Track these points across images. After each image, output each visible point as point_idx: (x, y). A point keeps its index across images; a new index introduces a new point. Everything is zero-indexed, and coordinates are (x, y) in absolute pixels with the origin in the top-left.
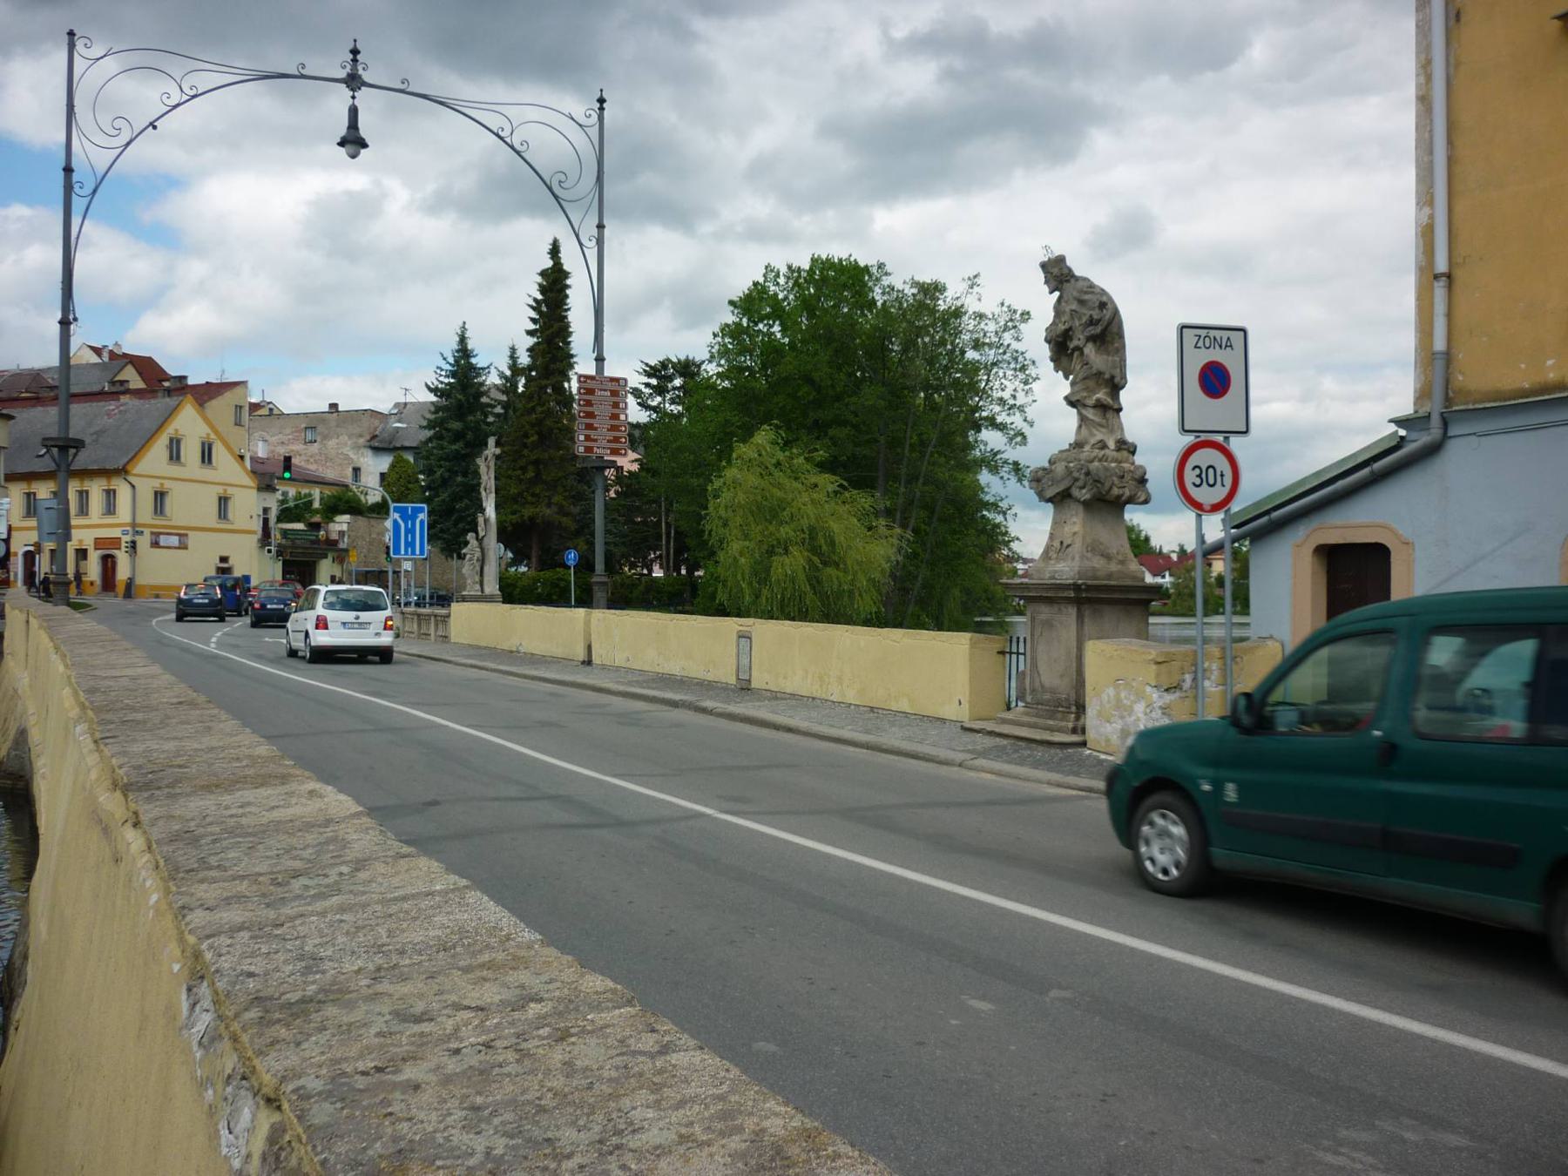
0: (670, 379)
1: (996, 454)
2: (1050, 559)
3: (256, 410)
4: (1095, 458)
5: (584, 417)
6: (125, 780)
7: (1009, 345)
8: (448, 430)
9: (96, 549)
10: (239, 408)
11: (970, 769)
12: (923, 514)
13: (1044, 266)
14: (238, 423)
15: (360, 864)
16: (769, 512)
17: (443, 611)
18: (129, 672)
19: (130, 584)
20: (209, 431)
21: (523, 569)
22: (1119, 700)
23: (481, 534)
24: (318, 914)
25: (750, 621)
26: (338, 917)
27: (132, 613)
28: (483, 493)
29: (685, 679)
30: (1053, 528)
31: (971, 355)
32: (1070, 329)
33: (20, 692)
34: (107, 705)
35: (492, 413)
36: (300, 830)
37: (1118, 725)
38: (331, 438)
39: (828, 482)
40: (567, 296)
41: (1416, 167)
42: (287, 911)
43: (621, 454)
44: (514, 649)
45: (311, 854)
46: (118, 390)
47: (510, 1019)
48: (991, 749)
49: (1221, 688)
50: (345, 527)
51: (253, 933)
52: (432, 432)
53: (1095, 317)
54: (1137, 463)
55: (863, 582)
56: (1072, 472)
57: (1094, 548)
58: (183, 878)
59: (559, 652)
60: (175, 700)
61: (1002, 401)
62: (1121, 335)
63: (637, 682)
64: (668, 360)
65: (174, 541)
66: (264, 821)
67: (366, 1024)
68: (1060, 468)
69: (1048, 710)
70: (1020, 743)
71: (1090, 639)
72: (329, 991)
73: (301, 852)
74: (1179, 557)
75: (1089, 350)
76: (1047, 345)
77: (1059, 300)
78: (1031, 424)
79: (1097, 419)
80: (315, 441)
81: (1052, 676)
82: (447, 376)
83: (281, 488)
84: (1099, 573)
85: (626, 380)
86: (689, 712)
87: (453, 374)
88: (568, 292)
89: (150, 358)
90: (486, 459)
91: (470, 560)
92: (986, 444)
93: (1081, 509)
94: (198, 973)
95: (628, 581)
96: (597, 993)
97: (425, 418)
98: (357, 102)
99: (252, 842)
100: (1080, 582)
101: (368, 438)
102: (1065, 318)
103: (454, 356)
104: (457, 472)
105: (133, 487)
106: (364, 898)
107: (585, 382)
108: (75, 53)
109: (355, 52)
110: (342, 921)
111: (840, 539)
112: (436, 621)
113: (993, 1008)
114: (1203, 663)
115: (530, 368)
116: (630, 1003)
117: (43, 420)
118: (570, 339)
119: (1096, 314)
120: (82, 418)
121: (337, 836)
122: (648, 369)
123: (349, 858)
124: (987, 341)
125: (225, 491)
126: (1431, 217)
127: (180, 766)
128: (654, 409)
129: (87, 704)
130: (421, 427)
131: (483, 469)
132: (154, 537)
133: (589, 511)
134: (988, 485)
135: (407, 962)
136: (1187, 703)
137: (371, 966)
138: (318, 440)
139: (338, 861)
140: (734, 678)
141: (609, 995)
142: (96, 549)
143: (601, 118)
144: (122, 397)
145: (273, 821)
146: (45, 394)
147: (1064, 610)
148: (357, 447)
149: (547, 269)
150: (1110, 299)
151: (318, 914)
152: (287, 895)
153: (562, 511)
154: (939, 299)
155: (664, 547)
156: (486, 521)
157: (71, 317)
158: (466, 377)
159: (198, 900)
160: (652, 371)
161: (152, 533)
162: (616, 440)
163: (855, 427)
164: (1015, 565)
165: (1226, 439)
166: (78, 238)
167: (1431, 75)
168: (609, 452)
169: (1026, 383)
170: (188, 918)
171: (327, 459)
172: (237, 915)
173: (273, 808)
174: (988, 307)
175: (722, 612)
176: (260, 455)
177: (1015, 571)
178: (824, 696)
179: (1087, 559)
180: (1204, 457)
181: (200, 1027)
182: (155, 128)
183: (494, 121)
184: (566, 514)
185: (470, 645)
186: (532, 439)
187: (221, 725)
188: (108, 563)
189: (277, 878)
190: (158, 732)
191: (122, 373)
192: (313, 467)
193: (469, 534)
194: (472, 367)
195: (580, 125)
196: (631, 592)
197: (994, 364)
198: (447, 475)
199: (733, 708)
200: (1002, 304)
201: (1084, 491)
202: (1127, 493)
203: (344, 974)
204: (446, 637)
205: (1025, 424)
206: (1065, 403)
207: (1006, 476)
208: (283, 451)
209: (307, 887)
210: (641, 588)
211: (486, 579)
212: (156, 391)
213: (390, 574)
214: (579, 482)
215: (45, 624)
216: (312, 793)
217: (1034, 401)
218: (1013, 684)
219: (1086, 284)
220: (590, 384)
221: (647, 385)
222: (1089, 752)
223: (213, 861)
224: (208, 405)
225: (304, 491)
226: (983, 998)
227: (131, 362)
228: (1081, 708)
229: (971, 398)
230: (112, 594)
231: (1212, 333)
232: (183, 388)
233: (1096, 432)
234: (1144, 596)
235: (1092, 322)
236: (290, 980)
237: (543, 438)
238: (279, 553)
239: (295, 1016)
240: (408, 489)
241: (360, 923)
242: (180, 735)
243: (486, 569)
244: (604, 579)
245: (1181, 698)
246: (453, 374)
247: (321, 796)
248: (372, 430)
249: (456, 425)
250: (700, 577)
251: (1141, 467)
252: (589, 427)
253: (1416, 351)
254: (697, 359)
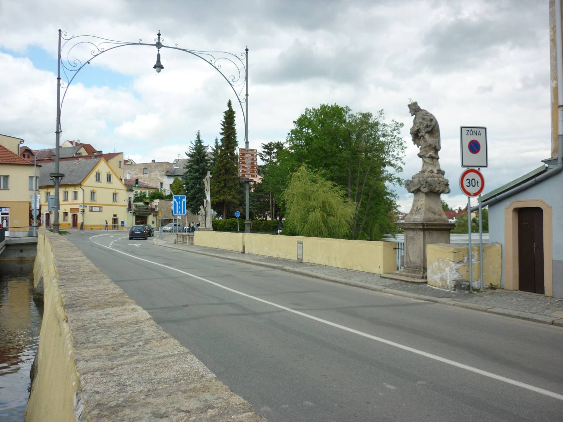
0: (272, 149)
1: (391, 175)
2: (413, 214)
3: (126, 163)
4: (429, 176)
5: (241, 164)
6: (65, 304)
7: (396, 136)
8: (193, 169)
9: (70, 212)
10: (120, 162)
11: (385, 292)
12: (365, 197)
13: (409, 106)
14: (120, 167)
15: (147, 342)
16: (306, 196)
17: (192, 234)
18: (74, 259)
19: (82, 225)
20: (110, 170)
21: (220, 218)
22: (439, 267)
23: (205, 206)
24: (128, 364)
25: (302, 237)
26: (136, 365)
27: (82, 235)
28: (206, 192)
29: (279, 258)
30: (414, 202)
31: (382, 139)
32: (419, 129)
33: (42, 264)
34: (64, 272)
35: (209, 163)
36: (126, 326)
37: (439, 276)
38: (153, 172)
39: (329, 184)
40: (234, 120)
41: (551, 66)
42: (116, 362)
43: (255, 177)
44: (217, 248)
45: (129, 336)
46: (79, 156)
47: (200, 417)
48: (391, 285)
49: (478, 262)
50: (157, 204)
51: (102, 373)
52: (188, 169)
53: (429, 124)
54: (445, 178)
55: (343, 222)
56: (421, 182)
57: (429, 210)
58: (79, 347)
59: (233, 249)
60: (89, 270)
61: (393, 156)
62: (438, 131)
63: (261, 259)
64: (271, 142)
65: (98, 209)
66: (113, 321)
67: (140, 418)
68: (416, 180)
69: (412, 270)
70: (402, 282)
71: (428, 244)
72: (128, 401)
73: (125, 335)
74: (458, 212)
75: (427, 136)
76: (411, 135)
77: (415, 118)
78: (404, 164)
79: (430, 162)
80: (147, 173)
81: (414, 258)
82: (193, 150)
83: (135, 190)
84: (432, 219)
85: (256, 150)
86: (279, 271)
87: (195, 149)
88: (235, 119)
89: (90, 145)
90: (207, 179)
91: (201, 215)
92: (388, 172)
93: (424, 196)
94: (80, 390)
95: (258, 222)
96: (236, 405)
97: (185, 165)
98: (160, 52)
99: (107, 331)
100: (424, 222)
101: (166, 172)
102: (418, 125)
103: (196, 143)
104: (197, 184)
105: (83, 190)
106: (147, 357)
107: (242, 151)
108: (61, 38)
110: (137, 367)
111: (335, 206)
112: (189, 238)
113: (396, 388)
114: (471, 252)
115: (222, 146)
116: (250, 410)
117: (50, 167)
118: (236, 136)
119: (429, 124)
120: (64, 167)
121: (140, 329)
122: (264, 146)
123: (143, 339)
124: (388, 134)
125: (115, 191)
126: (557, 84)
127: (86, 298)
128: (267, 160)
129: (57, 271)
130: (184, 168)
131: (206, 183)
132: (90, 208)
133: (244, 197)
134: (388, 186)
135: (161, 387)
136: (466, 267)
137: (146, 390)
138: (148, 173)
139: (139, 340)
140: (297, 258)
141: (241, 406)
142: (70, 212)
143: (247, 56)
144: (79, 159)
145: (116, 322)
146: (53, 158)
147: (418, 233)
148: (161, 175)
149: (227, 111)
150: (434, 118)
151: (128, 364)
152: (117, 355)
153: (234, 198)
154: (369, 119)
155: (271, 210)
156: (207, 201)
157: (60, 130)
158: (200, 150)
159: (83, 357)
160: (266, 147)
161: (90, 206)
162: (253, 172)
163: (340, 166)
164: (398, 215)
165: (479, 169)
166: (62, 103)
167: (555, 31)
168: (250, 176)
169: (402, 149)
170: (77, 365)
171: (152, 179)
172: (97, 364)
173: (117, 316)
174: (388, 121)
175: (293, 234)
176: (128, 178)
177: (398, 217)
178: (329, 265)
179: (427, 214)
180: (471, 176)
181: (80, 411)
182: (89, 63)
184: (236, 198)
185: (201, 246)
186: (223, 171)
187: (104, 281)
188: (75, 217)
189: (114, 347)
190: (80, 283)
191: (80, 150)
192: (146, 182)
193: (201, 206)
194: (202, 146)
195: (239, 59)
196: (259, 227)
197: (391, 142)
198: (193, 185)
199: (295, 269)
200: (393, 121)
201: (425, 189)
202: (441, 189)
203: (135, 393)
204: (193, 243)
205: (402, 164)
206: (417, 156)
207: (395, 183)
208: (136, 177)
209: (126, 351)
210: (263, 225)
211: (207, 222)
212: (91, 156)
213: (173, 220)
214: (241, 187)
215: (49, 240)
216: (133, 309)
217: (405, 156)
218: (400, 259)
219: (425, 112)
220: (244, 152)
221: (264, 152)
222: (428, 286)
223: (91, 339)
224: (109, 161)
225: (143, 191)
226: (392, 384)
227: (83, 146)
228: (425, 269)
229: (382, 155)
230: (76, 228)
231: (473, 129)
232: (101, 155)
233: (429, 166)
234: (449, 228)
235: (427, 126)
236: (113, 396)
237: (227, 171)
238: (134, 213)
239: (112, 413)
240: (180, 190)
241: (144, 369)
242: (88, 284)
243: (207, 218)
244: (249, 222)
245: (463, 265)
246: (195, 149)
247: (136, 311)
248: (167, 169)
249: (196, 167)
250: (283, 221)
251: (447, 179)
252: (243, 167)
253: (552, 134)
254: (282, 142)
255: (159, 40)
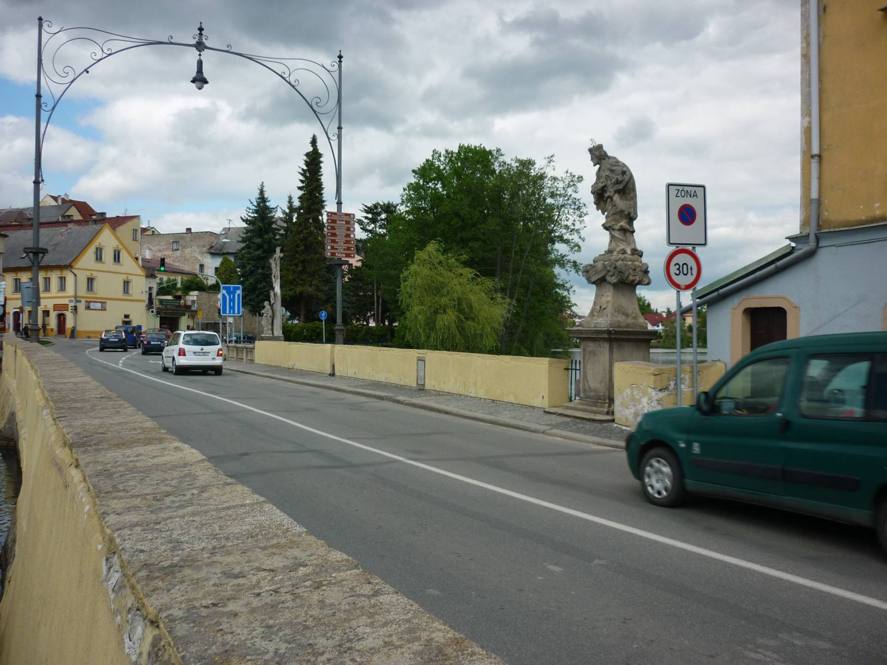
0: (379, 214)
1: (563, 257)
2: (594, 316)
3: (145, 232)
4: (619, 259)
5: (330, 236)
6: (71, 441)
7: (571, 195)
8: (253, 243)
9: (54, 310)
10: (135, 231)
11: (549, 435)
12: (522, 291)
13: (590, 150)
14: (135, 239)
15: (204, 489)
16: (435, 289)
17: (251, 346)
18: (73, 380)
19: (73, 330)
20: (118, 244)
21: (296, 322)
22: (633, 396)
23: (272, 302)
24: (180, 517)
25: (424, 351)
26: (191, 518)
27: (74, 347)
28: (273, 279)
29: (387, 384)
30: (596, 299)
31: (549, 201)
32: (605, 186)
33: (11, 391)
34: (60, 399)
35: (278, 234)
36: (170, 470)
37: (632, 410)
38: (187, 248)
39: (468, 272)
40: (321, 168)
41: (801, 94)
42: (162, 515)
43: (351, 257)
44: (291, 367)
45: (176, 483)
46: (67, 221)
47: (288, 576)
48: (560, 424)
49: (690, 389)
50: (195, 298)
51: (143, 528)
52: (244, 244)
53: (620, 179)
54: (643, 262)
55: (488, 329)
56: (606, 267)
57: (619, 310)
58: (103, 497)
59: (316, 369)
60: (99, 396)
61: (567, 227)
62: (634, 190)
63: (360, 385)
64: (378, 203)
65: (99, 306)
66: (150, 464)
67: (207, 579)
68: (599, 265)
69: (593, 402)
70: (577, 420)
71: (616, 361)
72: (186, 560)
73: (170, 482)
74: (667, 315)
75: (616, 198)
76: (592, 195)
77: (599, 170)
78: (583, 240)
79: (621, 237)
80: (178, 250)
81: (595, 382)
82: (253, 213)
83: (159, 276)
84: (622, 324)
85: (354, 215)
86: (390, 403)
87: (256, 212)
88: (321, 165)
89: (85, 202)
90: (275, 260)
91: (266, 316)
92: (558, 251)
93: (611, 288)
94: (112, 550)
95: (355, 329)
96: (337, 561)
97: (240, 236)
98: (202, 58)
99: (142, 476)
100: (611, 329)
101: (208, 247)
102: (603, 180)
103: (257, 202)
104: (258, 267)
105: (75, 275)
106: (206, 508)
107: (331, 216)
108: (43, 30)
109: (201, 29)
110: (193, 521)
111: (475, 305)
112: (247, 351)
113: (562, 570)
114: (681, 375)
115: (300, 208)
116: (356, 567)
117: (25, 237)
118: (322, 192)
119: (620, 178)
120: (46, 236)
121: (191, 473)
122: (366, 208)
123: (197, 485)
124: (559, 193)
125: (127, 277)
126: (810, 123)
127: (102, 433)
128: (370, 231)
129: (49, 398)
130: (238, 242)
131: (273, 265)
132: (87, 304)
133: (333, 289)
134: (559, 274)
135: (230, 544)
136: (671, 397)
137: (210, 547)
138: (180, 249)
139: (191, 487)
140: (415, 383)
141: (344, 563)
142: (54, 310)
143: (340, 67)
144: (69, 224)
145: (154, 464)
146: (25, 223)
147: (602, 345)
148: (202, 253)
149: (310, 152)
150: (628, 169)
151: (180, 517)
152: (162, 506)
153: (318, 289)
154: (531, 169)
155: (376, 310)
156: (275, 295)
157: (40, 179)
158: (264, 213)
159: (112, 509)
160: (369, 210)
161: (86, 301)
162: (349, 249)
163: (484, 241)
164: (574, 319)
165: (694, 248)
166: (44, 134)
167: (809, 42)
168: (344, 255)
169: (580, 216)
170: (107, 519)
171: (185, 260)
172: (134, 517)
173: (154, 457)
174: (559, 174)
175: (409, 346)
176: (147, 257)
177: (574, 323)
178: (466, 394)
179: (615, 316)
180: (681, 258)
181: (113, 581)
182: (88, 72)
183: (279, 69)
184: (320, 291)
185: (266, 365)
186: (301, 248)
187: (125, 410)
188: (61, 319)
189: (156, 497)
190: (89, 414)
191: (69, 211)
192: (177, 264)
193: (266, 302)
194: (267, 208)
195: (328, 71)
196: (357, 335)
197: (562, 206)
198: (253, 269)
199: (414, 401)
200: (567, 172)
201: (613, 278)
202: (638, 279)
203: (194, 551)
204: (252, 360)
205: (580, 240)
206: (602, 228)
207: (569, 269)
208: (160, 255)
209: (173, 502)
210: (363, 332)
211: (275, 327)
212: (88, 221)
213: (221, 324)
214: (328, 272)
215: (25, 353)
216: (176, 448)
217: (585, 227)
218: (573, 387)
219: (614, 161)
220: (334, 217)
221: (366, 218)
222: (616, 425)
223: (121, 487)
224: (117, 229)
225: (172, 278)
226: (556, 564)
227: (74, 205)
228: (611, 400)
229: (549, 225)
230: (64, 336)
231: (686, 188)
232: (104, 220)
233: (620, 244)
234: (647, 337)
235: (618, 182)
236: (164, 554)
237: (307, 248)
238: (158, 313)
239: (167, 574)
240: (231, 277)
241: (204, 522)
242: (102, 416)
243: (275, 322)
244: (342, 328)
245: (668, 394)
246: (256, 212)
247: (182, 450)
248: (210, 243)
249: (258, 240)
250: (396, 326)
251: (646, 264)
252: (333, 241)
253: (801, 198)
254: (395, 203)
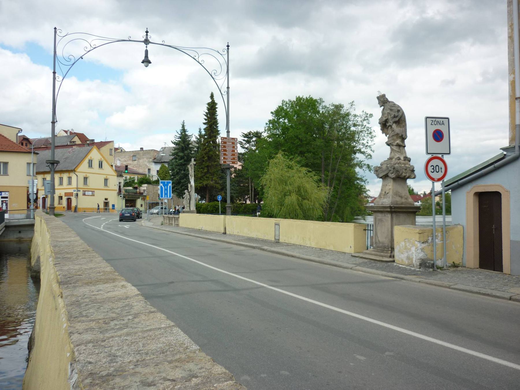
0: (252, 138)
1: (361, 162)
2: (381, 198)
3: (116, 151)
4: (397, 163)
5: (223, 151)
6: (60, 281)
7: (365, 125)
8: (178, 156)
9: (65, 196)
10: (111, 150)
11: (355, 270)
12: (337, 182)
13: (378, 98)
14: (111, 155)
15: (136, 316)
16: (283, 181)
17: (177, 216)
18: (69, 239)
19: (76, 208)
20: (101, 157)
21: (204, 202)
22: (406, 246)
23: (189, 190)
24: (119, 336)
25: (279, 219)
26: (125, 338)
27: (76, 217)
28: (190, 177)
29: (257, 239)
30: (382, 187)
31: (353, 129)
32: (387, 119)
33: (38, 244)
34: (59, 252)
35: (193, 150)
36: (117, 301)
37: (406, 255)
38: (141, 159)
39: (304, 170)
40: (217, 111)
41: (509, 61)
42: (107, 335)
43: (235, 164)
44: (200, 229)
45: (119, 311)
46: (73, 144)
47: (184, 386)
48: (361, 263)
49: (442, 242)
50: (145, 188)
51: (94, 344)
52: (174, 157)
53: (396, 115)
54: (411, 165)
55: (317, 205)
56: (388, 168)
57: (397, 194)
58: (73, 320)
59: (215, 230)
60: (82, 250)
61: (363, 144)
62: (405, 121)
63: (241, 240)
64: (251, 132)
65: (90, 193)
66: (105, 297)
67: (130, 386)
68: (384, 167)
69: (381, 250)
70: (372, 261)
71: (395, 225)
72: (118, 371)
73: (115, 310)
74: (423, 196)
75: (394, 126)
76: (379, 125)
77: (383, 109)
78: (373, 151)
79: (397, 150)
80: (136, 160)
81: (383, 238)
82: (178, 138)
83: (125, 176)
84: (399, 203)
85: (237, 139)
86: (258, 250)
87: (180, 138)
88: (217, 110)
89: (83, 134)
90: (191, 166)
91: (186, 199)
92: (358, 159)
93: (392, 181)
94: (74, 361)
95: (238, 206)
96: (218, 374)
97: (171, 153)
98: (148, 48)
99: (99, 306)
100: (392, 206)
101: (153, 159)
102: (386, 115)
103: (181, 132)
104: (182, 170)
105: (77, 176)
106: (136, 330)
107: (223, 139)
108: (57, 35)
110: (127, 340)
111: (309, 191)
112: (175, 220)
113: (365, 359)
114: (435, 233)
115: (205, 135)
116: (231, 379)
117: (46, 154)
118: (218, 126)
119: (396, 114)
120: (59, 154)
121: (129, 304)
122: (244, 135)
123: (132, 313)
124: (358, 124)
125: (107, 177)
126: (514, 78)
127: (79, 275)
128: (247, 148)
129: (53, 251)
130: (170, 155)
131: (190, 169)
132: (84, 192)
133: (225, 182)
134: (358, 172)
135: (148, 358)
136: (430, 247)
137: (135, 360)
138: (137, 160)
139: (128, 314)
140: (274, 239)
141: (223, 375)
142: (65, 196)
143: (228, 52)
144: (73, 147)
145: (107, 297)
146: (49, 146)
147: (386, 215)
148: (149, 162)
149: (210, 103)
150: (401, 109)
151: (119, 336)
152: (108, 328)
153: (216, 183)
154: (341, 110)
155: (250, 194)
156: (191, 186)
157: (55, 121)
158: (184, 139)
159: (77, 329)
160: (246, 136)
161: (83, 191)
162: (234, 159)
163: (314, 153)
164: (368, 199)
165: (443, 156)
166: (57, 95)
167: (513, 29)
168: (231, 163)
169: (371, 138)
170: (72, 338)
171: (140, 166)
172: (89, 336)
173: (108, 292)
174: (358, 112)
175: (271, 216)
176: (118, 165)
177: (368, 201)
178: (304, 245)
179: (394, 198)
180: (435, 162)
181: (74, 380)
182: (82, 58)
184: (218, 183)
185: (186, 228)
186: (206, 158)
187: (96, 259)
188: (69, 201)
189: (106, 321)
190: (74, 262)
191: (73, 139)
192: (135, 169)
193: (186, 190)
194: (186, 135)
195: (221, 54)
196: (239, 209)
197: (361, 131)
198: (178, 171)
199: (273, 249)
200: (363, 112)
201: (393, 174)
202: (408, 175)
203: (125, 363)
204: (178, 225)
205: (371, 152)
206: (386, 144)
207: (365, 169)
208: (125, 163)
209: (116, 325)
210: (243, 208)
211: (191, 205)
212: (84, 145)
213: (160, 203)
214: (222, 173)
215: (45, 222)
216: (123, 286)
217: (374, 144)
218: (369, 240)
219: (393, 103)
220: (225, 140)
221: (244, 140)
222: (396, 264)
223: (84, 313)
224: (101, 149)
225: (132, 177)
226: (362, 355)
227: (77, 135)
228: (393, 249)
229: (353, 143)
230: (70, 211)
231: (437, 120)
232: (93, 143)
233: (396, 154)
234: (414, 210)
235: (395, 117)
236: (104, 366)
237: (210, 158)
238: (124, 197)
239: (104, 382)
240: (166, 176)
241: (133, 341)
242: (81, 263)
243: (191, 202)
244: (230, 205)
245: (428, 245)
246: (180, 138)
247: (126, 287)
248: (154, 156)
249: (181, 154)
250: (262, 204)
251: (413, 166)
252: (225, 154)
253: (509, 124)
254: (260, 131)
255: (147, 37)
